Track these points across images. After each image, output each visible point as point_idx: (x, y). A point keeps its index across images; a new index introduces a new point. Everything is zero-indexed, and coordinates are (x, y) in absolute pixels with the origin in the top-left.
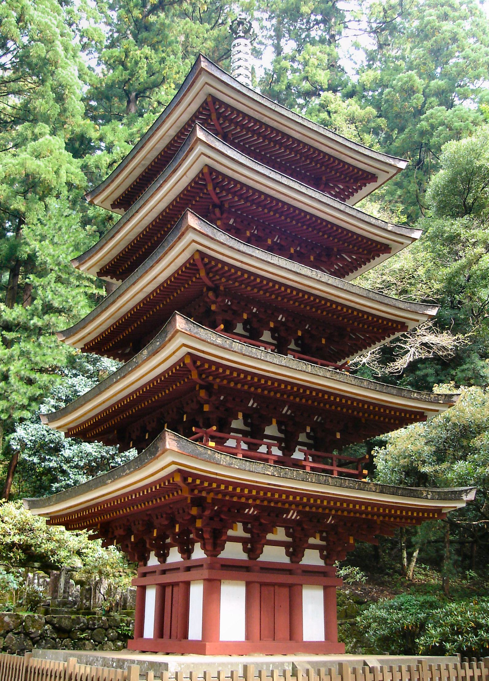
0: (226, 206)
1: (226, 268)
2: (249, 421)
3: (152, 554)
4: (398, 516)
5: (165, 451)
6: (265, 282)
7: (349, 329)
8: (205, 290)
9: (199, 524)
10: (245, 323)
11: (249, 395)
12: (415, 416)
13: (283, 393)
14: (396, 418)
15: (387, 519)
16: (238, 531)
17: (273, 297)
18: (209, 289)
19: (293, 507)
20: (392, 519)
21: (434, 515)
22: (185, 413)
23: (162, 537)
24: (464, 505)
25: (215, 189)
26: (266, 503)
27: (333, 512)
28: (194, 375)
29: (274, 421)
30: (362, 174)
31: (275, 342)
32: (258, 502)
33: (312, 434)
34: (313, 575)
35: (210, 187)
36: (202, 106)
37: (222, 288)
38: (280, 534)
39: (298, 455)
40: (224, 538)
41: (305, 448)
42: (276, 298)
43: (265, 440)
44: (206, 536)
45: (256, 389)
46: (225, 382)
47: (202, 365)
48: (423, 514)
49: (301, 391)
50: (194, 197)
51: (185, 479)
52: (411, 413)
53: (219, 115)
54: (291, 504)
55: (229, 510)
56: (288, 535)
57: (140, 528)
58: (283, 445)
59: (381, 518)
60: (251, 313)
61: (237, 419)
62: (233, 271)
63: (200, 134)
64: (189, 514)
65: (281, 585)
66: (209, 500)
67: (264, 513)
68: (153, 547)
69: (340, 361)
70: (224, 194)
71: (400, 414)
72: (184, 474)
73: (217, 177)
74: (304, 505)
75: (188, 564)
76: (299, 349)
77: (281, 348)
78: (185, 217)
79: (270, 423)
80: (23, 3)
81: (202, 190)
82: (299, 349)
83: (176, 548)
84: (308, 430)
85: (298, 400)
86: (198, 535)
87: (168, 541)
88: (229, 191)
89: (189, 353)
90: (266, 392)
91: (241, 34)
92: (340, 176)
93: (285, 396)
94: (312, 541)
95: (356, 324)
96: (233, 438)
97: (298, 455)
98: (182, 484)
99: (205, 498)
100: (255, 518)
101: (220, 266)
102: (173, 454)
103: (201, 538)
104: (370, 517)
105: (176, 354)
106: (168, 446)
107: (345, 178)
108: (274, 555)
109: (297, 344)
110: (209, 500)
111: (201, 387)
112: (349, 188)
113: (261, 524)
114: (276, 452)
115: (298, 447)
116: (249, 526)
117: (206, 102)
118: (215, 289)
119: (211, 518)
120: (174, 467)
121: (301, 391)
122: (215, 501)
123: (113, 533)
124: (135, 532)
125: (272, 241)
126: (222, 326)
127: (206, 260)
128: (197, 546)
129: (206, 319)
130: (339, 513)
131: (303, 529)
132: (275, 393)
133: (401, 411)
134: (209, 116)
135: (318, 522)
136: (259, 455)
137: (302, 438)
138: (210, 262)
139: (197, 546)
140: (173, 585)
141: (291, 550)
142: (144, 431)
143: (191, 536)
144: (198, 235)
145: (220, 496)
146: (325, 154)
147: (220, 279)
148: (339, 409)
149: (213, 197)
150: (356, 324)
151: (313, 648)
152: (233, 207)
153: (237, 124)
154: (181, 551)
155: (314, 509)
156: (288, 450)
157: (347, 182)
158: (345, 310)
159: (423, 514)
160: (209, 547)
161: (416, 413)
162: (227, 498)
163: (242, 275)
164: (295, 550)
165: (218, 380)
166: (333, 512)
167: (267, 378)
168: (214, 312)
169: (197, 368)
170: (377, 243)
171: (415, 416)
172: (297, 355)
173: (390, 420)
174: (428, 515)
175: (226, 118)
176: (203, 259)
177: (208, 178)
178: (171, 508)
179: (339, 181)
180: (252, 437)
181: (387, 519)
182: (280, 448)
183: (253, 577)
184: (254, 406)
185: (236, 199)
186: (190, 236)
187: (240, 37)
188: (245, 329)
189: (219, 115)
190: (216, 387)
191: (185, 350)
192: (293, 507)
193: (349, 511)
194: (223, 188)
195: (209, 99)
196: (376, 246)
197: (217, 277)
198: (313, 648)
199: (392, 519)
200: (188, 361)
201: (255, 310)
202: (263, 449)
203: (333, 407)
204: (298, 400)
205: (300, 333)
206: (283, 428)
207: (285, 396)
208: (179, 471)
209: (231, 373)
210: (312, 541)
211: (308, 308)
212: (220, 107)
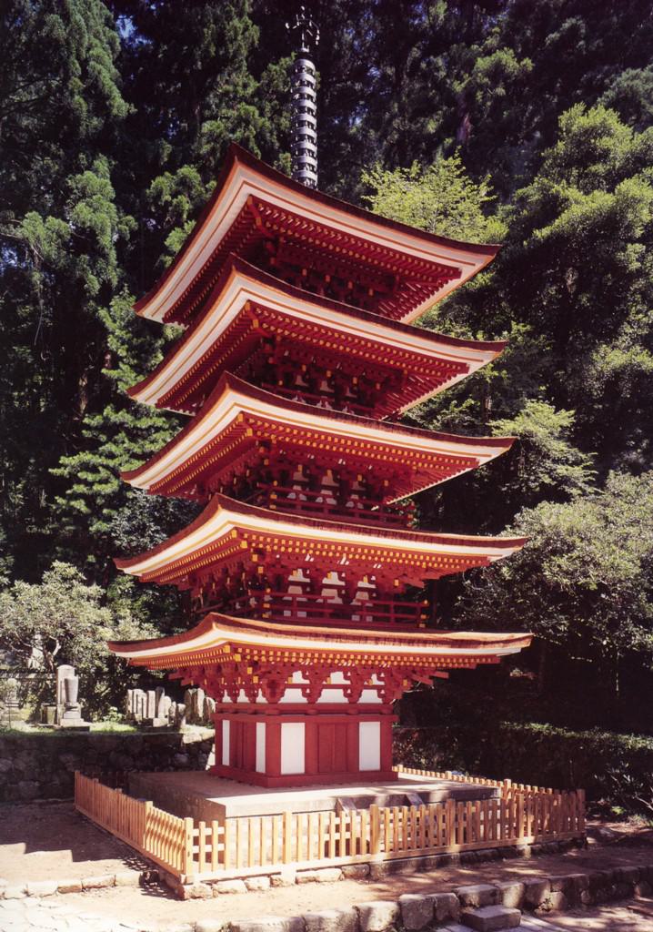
84: (360, 478)
107: (422, 276)
108: (331, 696)
169: (258, 316)
200: (234, 534)
208: (236, 528)
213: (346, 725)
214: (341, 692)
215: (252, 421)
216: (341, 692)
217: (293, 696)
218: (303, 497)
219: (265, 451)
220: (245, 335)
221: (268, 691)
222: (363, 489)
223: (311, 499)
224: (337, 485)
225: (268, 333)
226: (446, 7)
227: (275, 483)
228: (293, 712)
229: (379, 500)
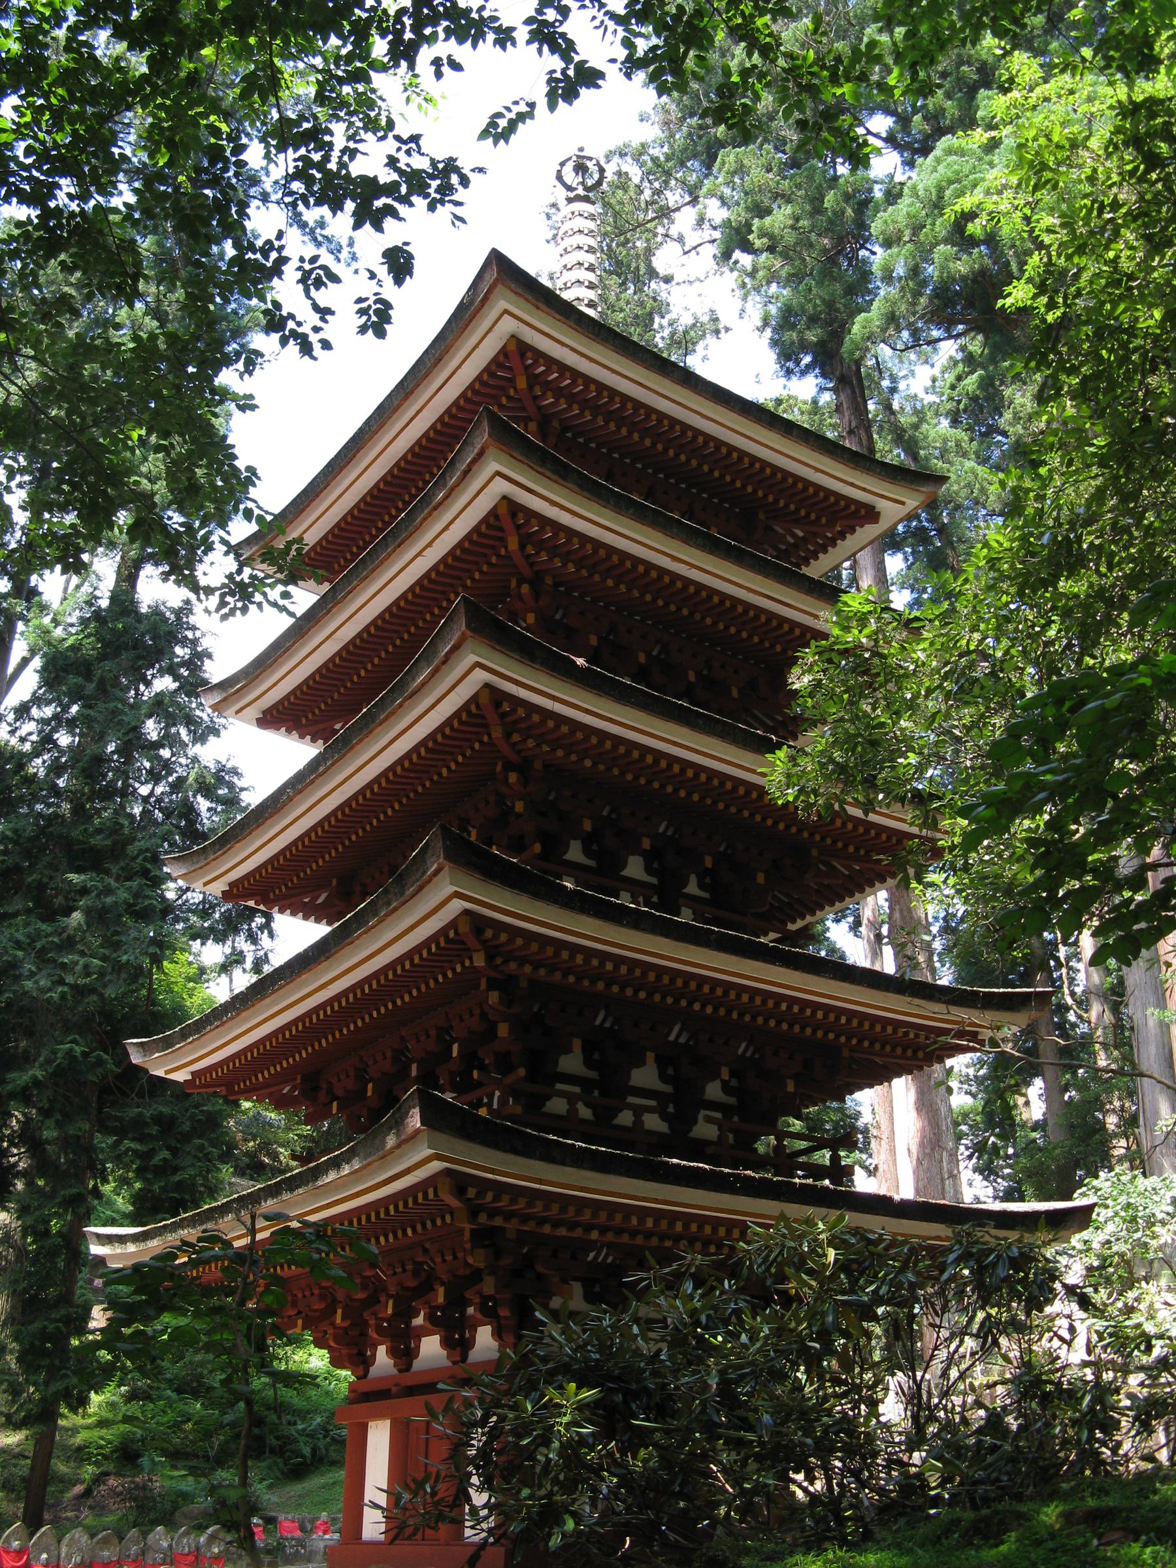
0: (549, 580)
2: (596, 1056)
10: (650, 859)
22: (454, 1040)
23: (405, 1313)
29: (650, 1056)
37: (538, 765)
41: (719, 1115)
43: (559, 1086)
44: (504, 1312)
53: (533, 380)
58: (671, 1109)
69: (794, 922)
73: (527, 522)
79: (641, 1063)
87: (419, 1321)
89: (466, 912)
90: (615, 989)
96: (562, 1094)
99: (502, 1230)
103: (489, 1314)
111: (493, 984)
112: (815, 535)
115: (703, 1113)
117: (503, 351)
126: (537, 848)
127: (506, 707)
137: (713, 1091)
143: (471, 1310)
146: (626, 398)
154: (446, 1343)
157: (813, 523)
163: (557, 727)
177: (507, 524)
179: (798, 522)
182: (664, 1117)
184: (682, 1040)
188: (587, 852)
189: (533, 380)
190: (523, 983)
191: (458, 905)
194: (541, 545)
197: (545, 748)
200: (464, 928)
202: (625, 1118)
205: (708, 862)
212: (536, 364)
215: (506, 707)
218: (585, 1112)
223: (605, 1115)
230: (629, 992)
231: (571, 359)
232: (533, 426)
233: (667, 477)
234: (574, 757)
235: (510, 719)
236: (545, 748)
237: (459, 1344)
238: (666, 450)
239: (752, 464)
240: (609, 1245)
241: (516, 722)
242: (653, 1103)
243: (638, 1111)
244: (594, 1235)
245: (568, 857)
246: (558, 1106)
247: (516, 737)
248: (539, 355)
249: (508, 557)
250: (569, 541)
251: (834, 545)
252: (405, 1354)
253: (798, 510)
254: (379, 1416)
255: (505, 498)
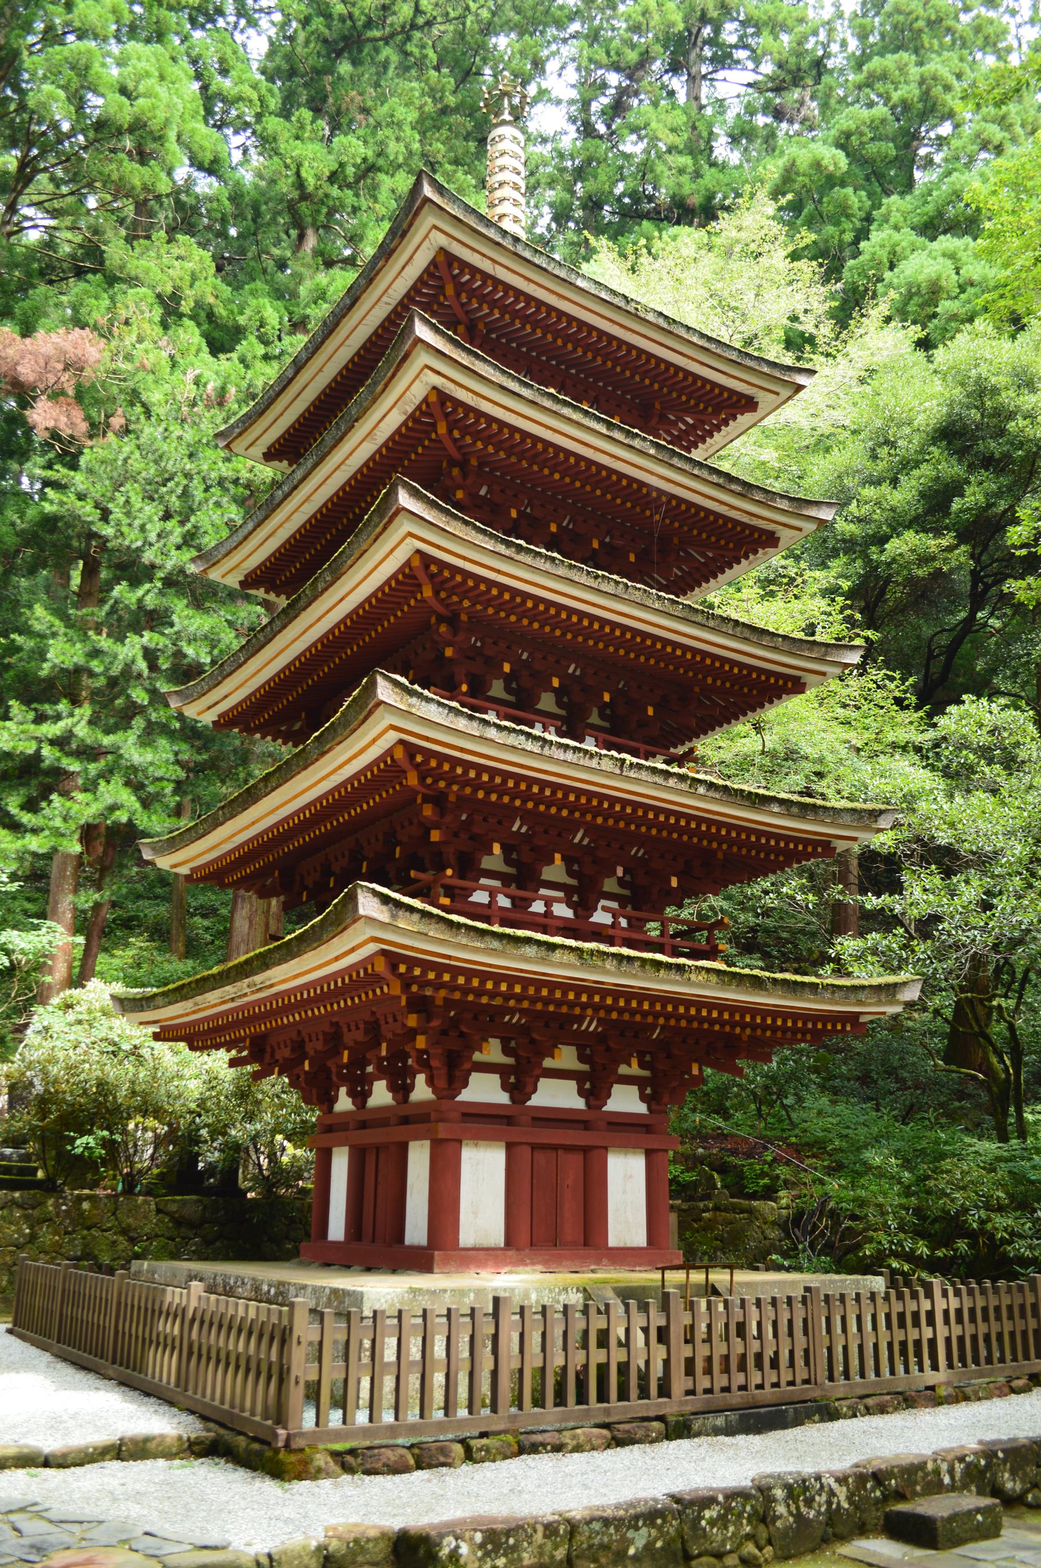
0: (474, 462)
1: (471, 583)
2: (514, 856)
3: (343, 1090)
4: (779, 1028)
5: (357, 918)
6: (542, 607)
7: (697, 689)
8: (433, 620)
9: (421, 1042)
10: (508, 679)
11: (511, 813)
12: (815, 849)
13: (573, 808)
14: (778, 851)
15: (759, 1032)
16: (493, 1052)
17: (558, 633)
18: (441, 619)
19: (589, 1012)
20: (768, 1033)
21: (844, 1026)
23: (359, 1062)
24: (899, 1009)
25: (450, 432)
26: (539, 1006)
27: (661, 1021)
28: (412, 779)
29: (558, 856)
30: (730, 398)
31: (563, 712)
32: (525, 1004)
33: (628, 878)
34: (626, 1130)
35: (442, 428)
36: (426, 270)
37: (464, 617)
38: (566, 1057)
39: (601, 917)
40: (467, 1066)
42: (564, 634)
44: (435, 1063)
45: (524, 802)
46: (468, 790)
47: (426, 762)
48: (824, 1025)
49: (606, 805)
50: (407, 453)
51: (394, 968)
52: (806, 842)
53: (460, 288)
54: (584, 1007)
55: (475, 1018)
56: (581, 1058)
57: (319, 1046)
58: (575, 898)
59: (748, 1031)
60: (516, 663)
61: (491, 853)
62: (483, 587)
63: (422, 331)
64: (404, 1025)
65: (569, 1149)
66: (439, 1002)
67: (534, 1025)
68: (344, 1080)
70: (468, 440)
71: (787, 845)
72: (392, 959)
73: (455, 410)
74: (609, 1010)
75: (405, 1111)
76: (606, 724)
77: (572, 727)
78: (392, 493)
80: (11, 541)
81: (428, 433)
82: (606, 724)
83: (384, 1083)
84: (620, 872)
85: (600, 820)
86: (419, 1061)
87: (370, 1069)
88: (477, 435)
89: (401, 742)
91: (506, 116)
92: (688, 401)
93: (577, 815)
94: (623, 1070)
95: (710, 680)
96: (484, 888)
97: (601, 917)
98: (388, 975)
100: (523, 1030)
101: (459, 578)
102: (378, 921)
103: (424, 1065)
104: (727, 1029)
105: (379, 742)
106: (361, 912)
107: (697, 405)
108: (556, 1095)
109: (602, 716)
110: (439, 1002)
111: (426, 799)
112: (704, 423)
113: (533, 1041)
114: (562, 910)
115: (603, 902)
116: (513, 1044)
117: (433, 263)
118: (453, 620)
119: (444, 1033)
120: (372, 948)
121: (606, 805)
122: (448, 1003)
123: (272, 1055)
124: (312, 1053)
125: (559, 526)
127: (434, 568)
128: (421, 1079)
129: (432, 675)
130: (673, 1022)
131: (608, 1049)
132: (559, 810)
133: (788, 839)
134: (441, 289)
135: (636, 1036)
136: (529, 918)
138: (441, 572)
139: (421, 1079)
140: (378, 1149)
141: (587, 1086)
142: (327, 872)
144: (417, 529)
145: (457, 996)
146: (602, 333)
147: (461, 602)
148: (675, 836)
149: (446, 454)
150: (710, 680)
151: (625, 1256)
152: (487, 464)
153: (493, 304)
154: (392, 1088)
155: (626, 1017)
156: (584, 906)
157: (701, 412)
158: (689, 656)
159: (824, 1025)
160: (442, 1083)
161: (815, 843)
162: (471, 998)
164: (594, 1086)
165: (455, 788)
166: (661, 1021)
167: (543, 784)
168: (450, 659)
169: (417, 766)
170: (754, 529)
171: (815, 849)
172: (602, 736)
173: (767, 855)
174: (834, 1026)
175: (472, 293)
176: (427, 567)
177: (437, 411)
178: (373, 1013)
179: (688, 411)
180: (519, 887)
181: (759, 1032)
183: (516, 1134)
185: (491, 449)
186: (403, 526)
187: (504, 123)
188: (508, 689)
189: (460, 288)
190: (452, 798)
191: (393, 736)
192: (589, 1012)
193: (690, 1020)
194: (465, 430)
195: (441, 258)
196: (752, 534)
197: (455, 599)
198: (625, 1256)
199: (768, 1033)
200: (399, 754)
201: (525, 656)
202: (538, 907)
203: (665, 834)
204: (600, 820)
205: (607, 697)
206: (576, 867)
207: (577, 815)
208: (383, 952)
209: (479, 775)
210: (623, 1070)
211: (622, 652)
212: (462, 273)
213: (586, 1150)
214: (572, 1085)
215: (434, 568)
216: (572, 1085)
217: (484, 1090)
218: (504, 902)
219: (419, 1020)
220: (412, 602)
221: (441, 1073)
222: (626, 892)
223: (521, 904)
224: (585, 1067)
225: (447, 606)
226: (1010, 528)
227: (449, 872)
228: (484, 1122)
229: (657, 912)
230: (553, 810)
231: (486, 266)
232: (461, 329)
233: (624, 393)
234: (503, 614)
235: (437, 580)
236: (455, 599)
237: (401, 1089)
238: (633, 376)
239: (658, 365)
240: (522, 1011)
241: (443, 582)
242: (561, 894)
243: (548, 902)
244: (512, 1003)
245: (539, 706)
246: (480, 897)
247: (443, 595)
248: (464, 265)
249: (438, 441)
250: (489, 426)
251: (719, 430)
252: (360, 1096)
253: (688, 401)
254: (341, 1144)
255: (434, 388)
